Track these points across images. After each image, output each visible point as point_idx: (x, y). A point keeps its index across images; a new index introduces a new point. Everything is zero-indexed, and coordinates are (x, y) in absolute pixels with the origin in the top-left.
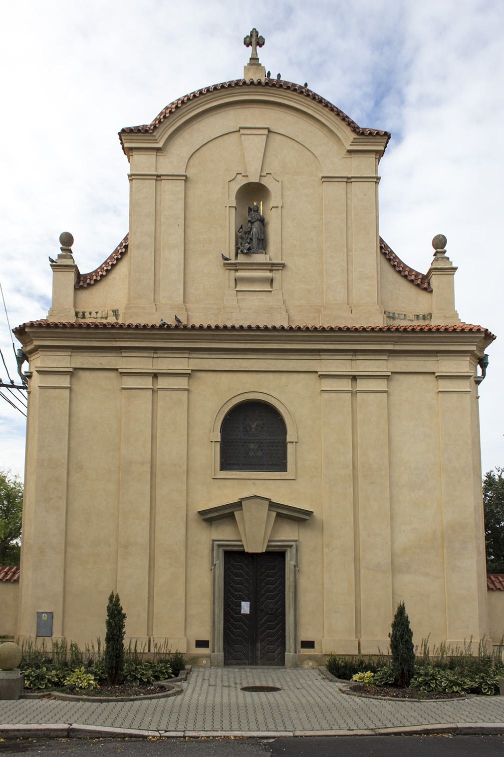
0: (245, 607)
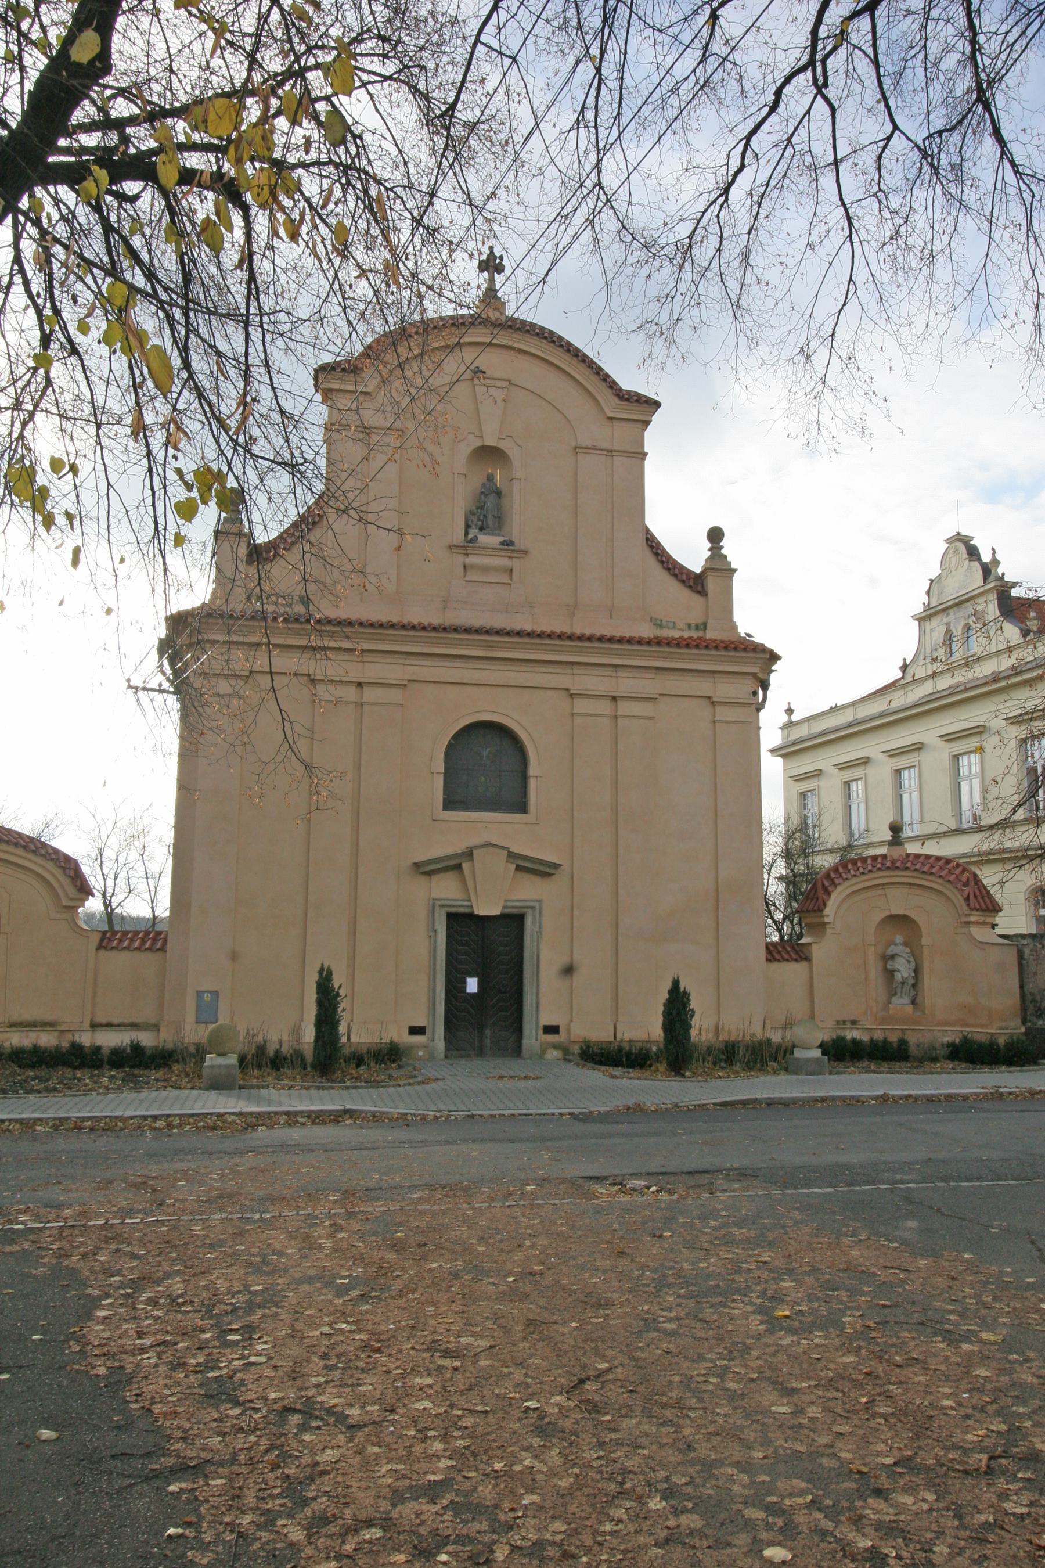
0: (472, 985)
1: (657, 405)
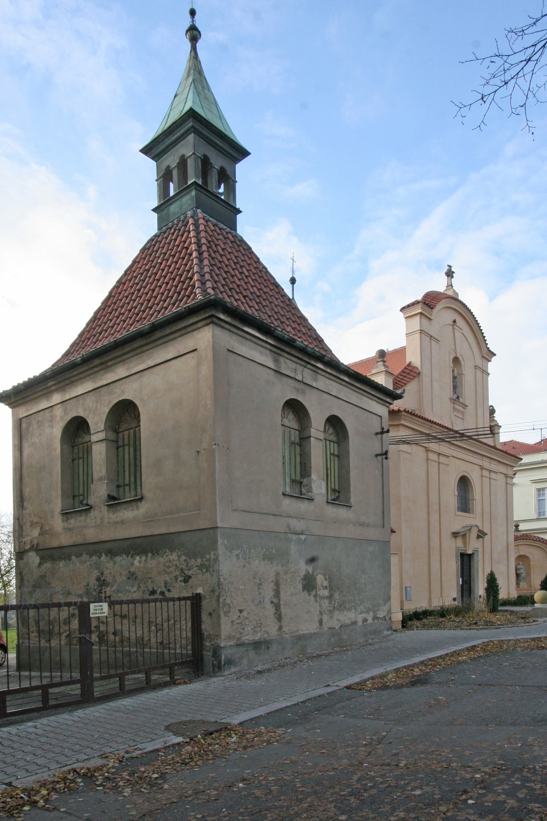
1: (495, 355)
